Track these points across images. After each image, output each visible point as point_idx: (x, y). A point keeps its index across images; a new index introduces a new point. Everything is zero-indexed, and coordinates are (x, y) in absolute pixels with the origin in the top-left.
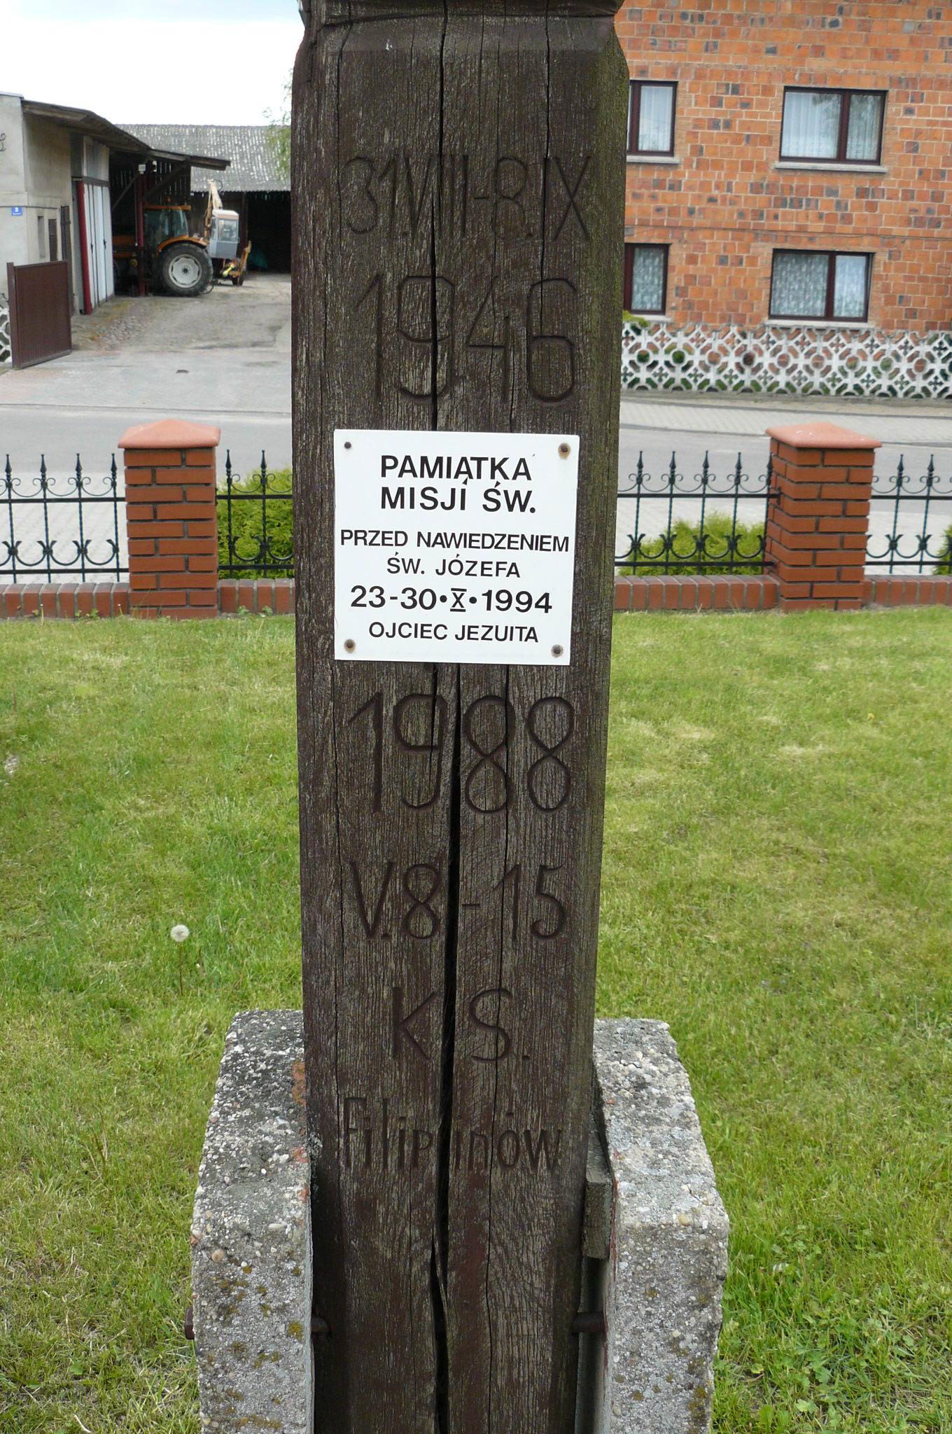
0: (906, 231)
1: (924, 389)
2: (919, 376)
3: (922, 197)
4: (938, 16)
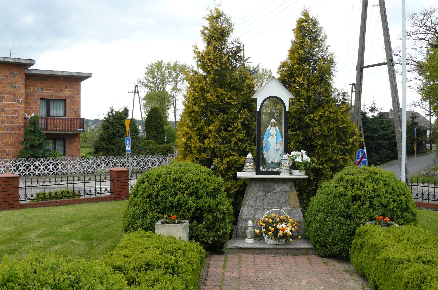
0: (4, 132)
1: (48, 173)
2: (73, 169)
3: (7, 123)
4: (7, 77)
